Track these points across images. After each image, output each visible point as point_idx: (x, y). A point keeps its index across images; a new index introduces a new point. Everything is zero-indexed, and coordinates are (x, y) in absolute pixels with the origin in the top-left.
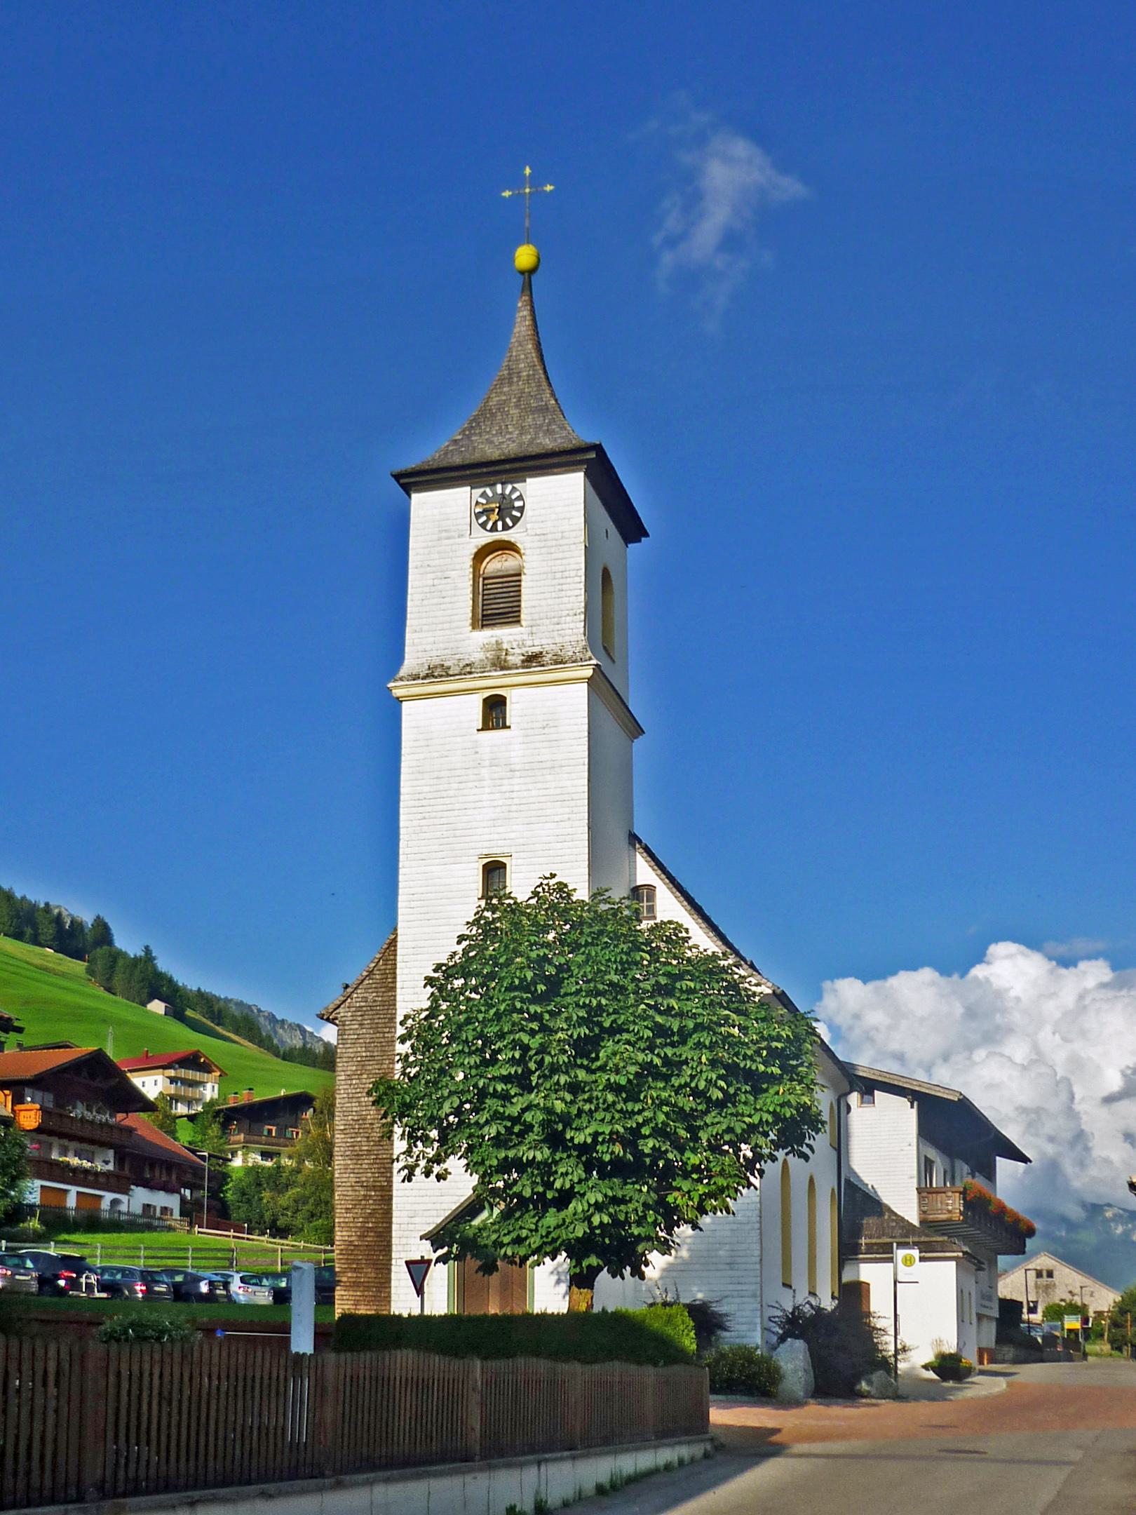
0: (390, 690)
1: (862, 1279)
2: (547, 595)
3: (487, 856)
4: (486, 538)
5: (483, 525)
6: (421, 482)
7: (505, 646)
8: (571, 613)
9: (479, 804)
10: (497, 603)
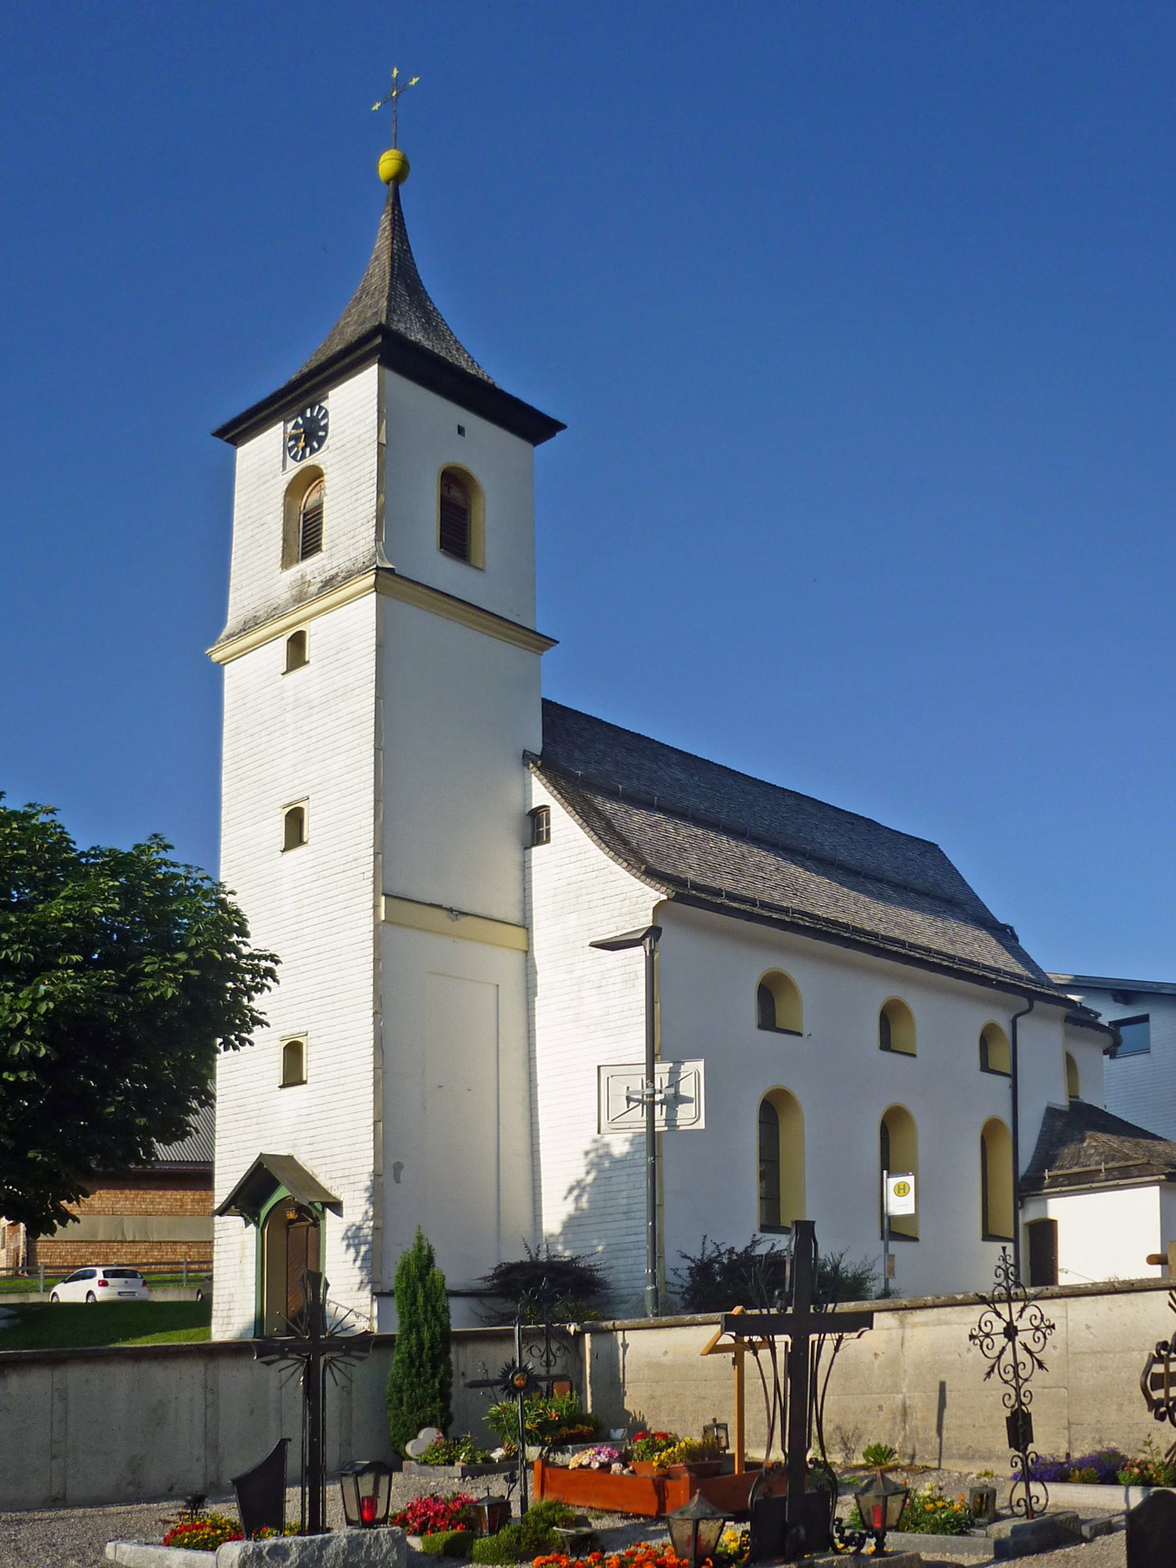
0: (208, 657)
1: (1051, 1216)
2: (344, 510)
3: (289, 805)
4: (294, 468)
5: (294, 458)
6: (245, 430)
7: (308, 578)
8: (365, 521)
9: (284, 752)
10: (305, 534)
